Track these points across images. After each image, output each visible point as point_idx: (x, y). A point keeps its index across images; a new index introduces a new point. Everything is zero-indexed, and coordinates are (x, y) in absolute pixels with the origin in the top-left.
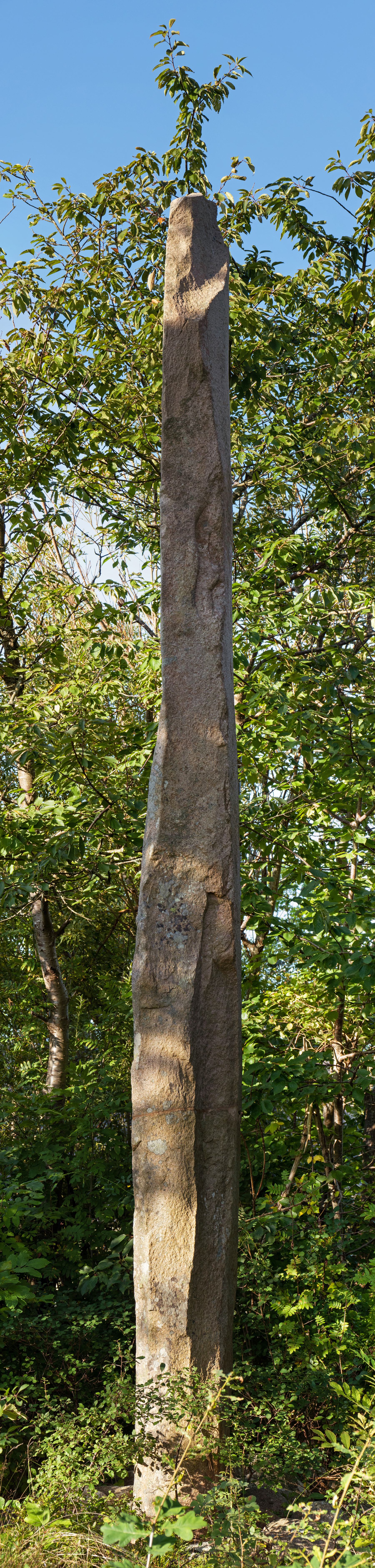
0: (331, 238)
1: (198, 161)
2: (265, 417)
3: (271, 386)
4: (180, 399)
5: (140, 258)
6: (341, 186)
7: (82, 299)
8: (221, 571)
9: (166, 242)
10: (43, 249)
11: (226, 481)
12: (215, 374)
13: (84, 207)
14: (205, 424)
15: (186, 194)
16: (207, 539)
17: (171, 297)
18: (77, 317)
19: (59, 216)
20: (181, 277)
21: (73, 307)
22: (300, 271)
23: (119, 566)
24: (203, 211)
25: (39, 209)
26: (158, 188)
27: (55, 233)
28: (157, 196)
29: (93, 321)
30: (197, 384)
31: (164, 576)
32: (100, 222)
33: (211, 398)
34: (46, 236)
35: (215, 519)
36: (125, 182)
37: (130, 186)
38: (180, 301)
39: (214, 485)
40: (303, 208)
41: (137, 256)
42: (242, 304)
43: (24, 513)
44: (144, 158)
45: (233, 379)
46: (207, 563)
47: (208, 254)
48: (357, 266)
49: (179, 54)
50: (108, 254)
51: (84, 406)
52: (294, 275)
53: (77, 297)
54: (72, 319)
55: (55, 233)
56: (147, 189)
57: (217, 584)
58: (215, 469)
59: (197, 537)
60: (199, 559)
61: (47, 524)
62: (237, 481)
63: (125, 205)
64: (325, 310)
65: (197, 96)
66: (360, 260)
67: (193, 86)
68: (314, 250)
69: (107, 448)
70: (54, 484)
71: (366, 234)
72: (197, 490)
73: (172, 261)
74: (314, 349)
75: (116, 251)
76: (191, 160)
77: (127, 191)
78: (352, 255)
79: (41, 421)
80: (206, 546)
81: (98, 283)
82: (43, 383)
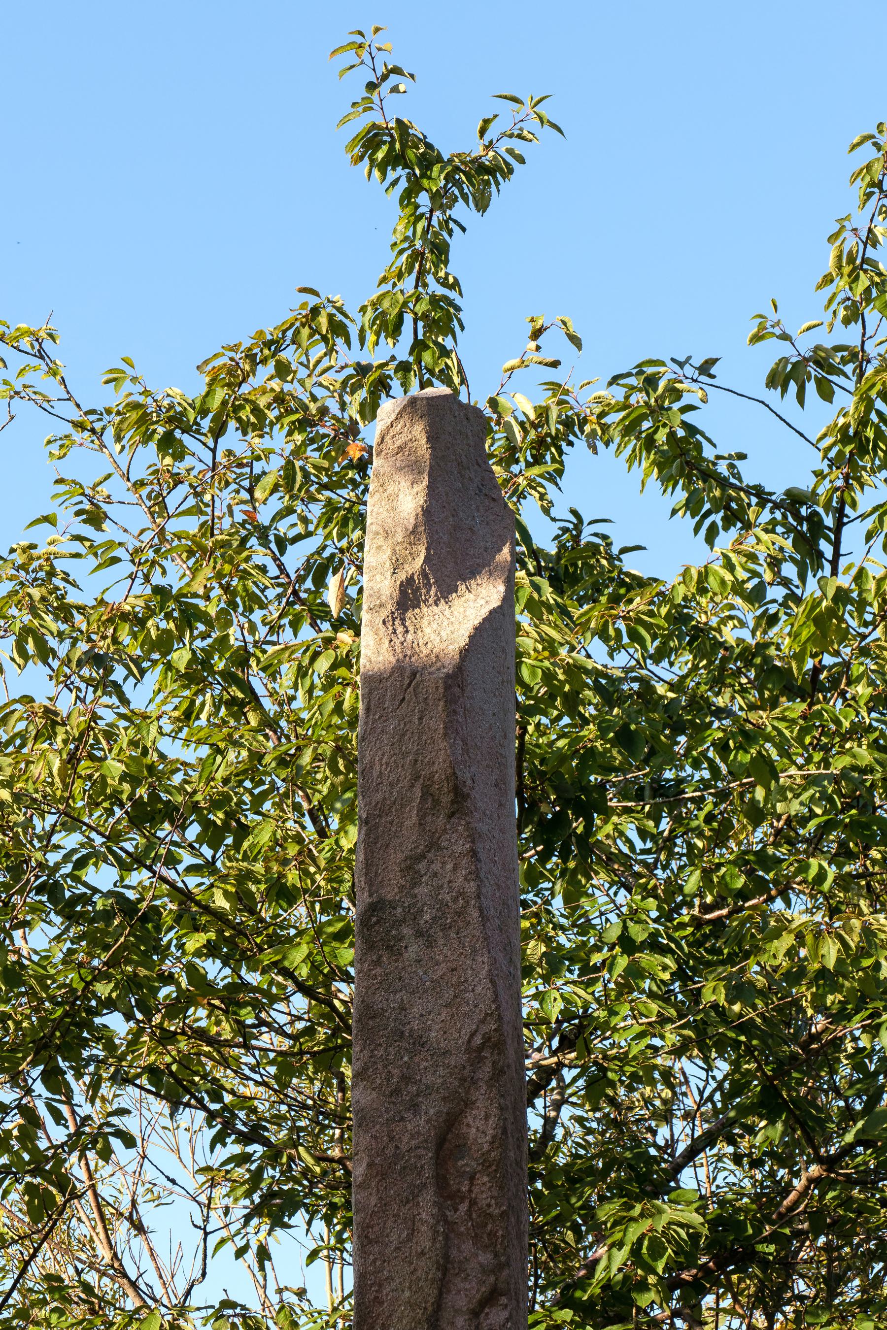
0: (761, 495)
1: (442, 318)
2: (607, 902)
3: (622, 830)
4: (400, 856)
5: (309, 534)
6: (778, 379)
7: (172, 625)
8: (501, 1267)
9: (367, 497)
10: (78, 513)
11: (511, 1052)
12: (482, 796)
13: (177, 420)
14: (458, 914)
15: (415, 390)
16: (464, 1189)
17: (379, 620)
18: (160, 667)
19: (118, 438)
20: (402, 576)
21: (152, 646)
22: (687, 570)
23: (251, 1256)
24: (457, 438)
25: (72, 422)
26: (350, 377)
27: (109, 476)
28: (347, 398)
29: (196, 675)
30: (441, 820)
31: (361, 1279)
32: (214, 451)
33: (473, 853)
34: (87, 483)
35: (484, 1142)
36: (272, 363)
37: (283, 370)
38: (400, 630)
39: (481, 1059)
40: (691, 430)
41: (300, 529)
42: (551, 646)
43: (20, 1127)
44: (315, 311)
45: (528, 813)
46: (467, 1247)
47: (467, 521)
48: (821, 555)
49: (395, 90)
50: (233, 525)
51: (171, 875)
52: (670, 577)
53: (156, 625)
54: (142, 672)
55: (109, 476)
56: (325, 380)
57: (490, 1299)
58: (483, 1021)
59: (441, 1182)
60: (447, 1238)
61: (75, 1155)
62: (539, 1050)
63: (272, 415)
64: (748, 655)
65: (434, 179)
66: (828, 539)
67: (430, 159)
68: (717, 518)
69: (227, 971)
70: (93, 1058)
71: (840, 483)
72: (441, 1071)
73: (380, 541)
74: (722, 748)
75: (251, 517)
76: (425, 316)
77: (275, 384)
78: (810, 527)
79: (70, 910)
80: (464, 1207)
81: (208, 590)
82: (71, 821)
